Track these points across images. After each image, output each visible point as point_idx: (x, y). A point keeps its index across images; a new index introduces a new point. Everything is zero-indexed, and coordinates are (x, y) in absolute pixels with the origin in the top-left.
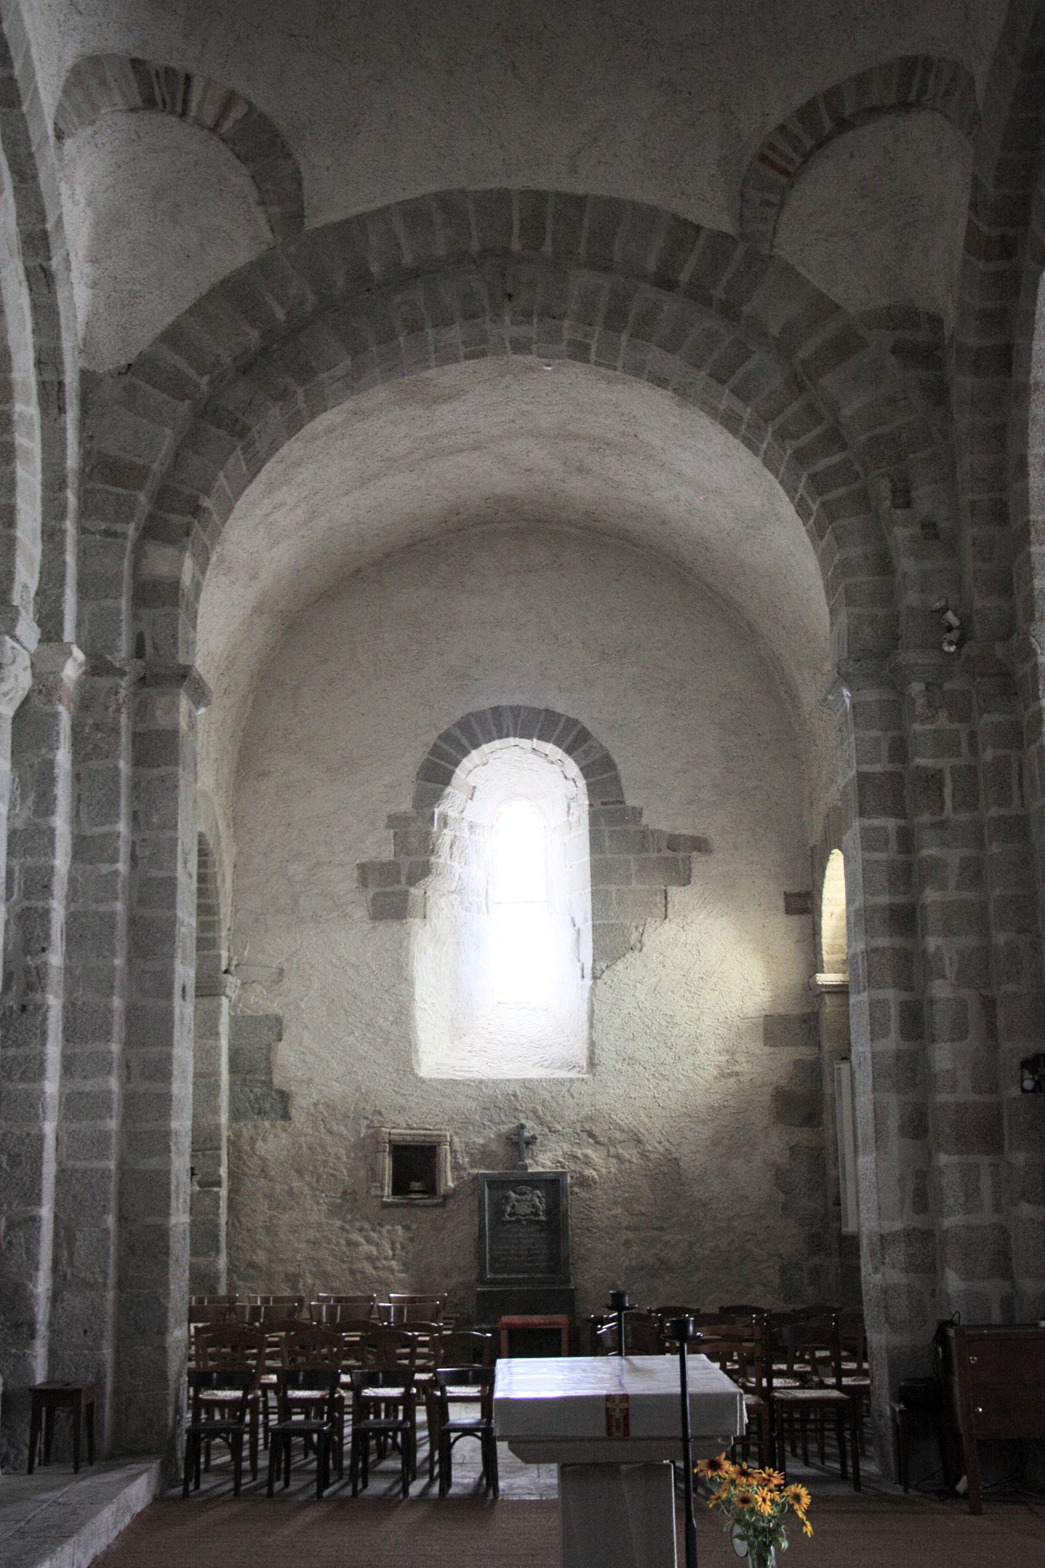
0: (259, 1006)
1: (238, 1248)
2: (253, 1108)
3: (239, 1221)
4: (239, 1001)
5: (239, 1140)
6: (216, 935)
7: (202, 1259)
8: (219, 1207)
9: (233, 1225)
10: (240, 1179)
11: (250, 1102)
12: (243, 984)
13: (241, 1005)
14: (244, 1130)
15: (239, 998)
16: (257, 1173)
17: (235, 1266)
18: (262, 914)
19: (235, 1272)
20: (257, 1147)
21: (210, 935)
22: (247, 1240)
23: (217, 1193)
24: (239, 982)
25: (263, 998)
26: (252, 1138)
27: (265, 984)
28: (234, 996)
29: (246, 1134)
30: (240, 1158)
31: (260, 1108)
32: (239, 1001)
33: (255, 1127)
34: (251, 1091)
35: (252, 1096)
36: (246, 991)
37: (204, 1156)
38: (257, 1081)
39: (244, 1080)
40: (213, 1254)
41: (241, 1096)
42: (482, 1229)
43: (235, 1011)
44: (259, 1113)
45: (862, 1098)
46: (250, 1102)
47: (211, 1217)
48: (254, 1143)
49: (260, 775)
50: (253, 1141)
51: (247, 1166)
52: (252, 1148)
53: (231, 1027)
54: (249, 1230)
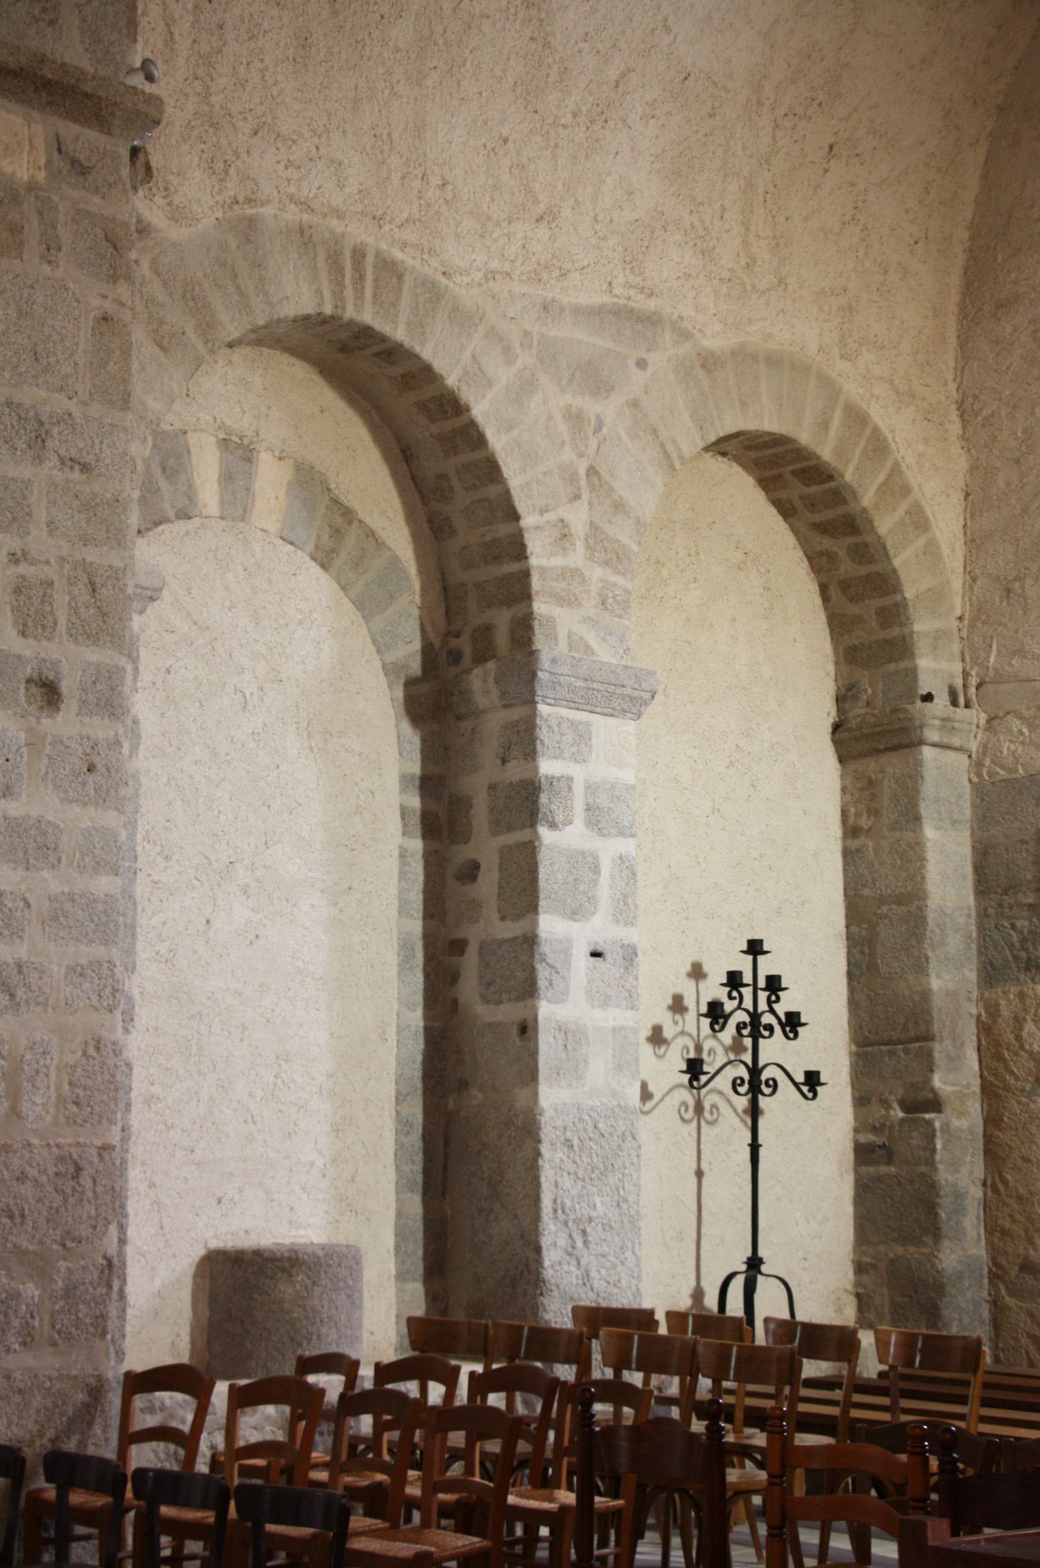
0: (1017, 759)
1: (1005, 1233)
2: (1016, 958)
3: (1005, 1182)
4: (985, 754)
5: (995, 1022)
6: (906, 631)
7: (912, 1249)
8: (934, 1150)
9: (995, 1189)
10: (998, 1096)
11: (1011, 947)
12: (989, 721)
13: (987, 762)
14: (1002, 1002)
15: (984, 748)
16: (1028, 1088)
17: (999, 1266)
18: (1017, 578)
19: (1001, 1279)
20: (1024, 1035)
21: (895, 632)
22: (1018, 1217)
23: (929, 1123)
24: (983, 717)
25: (1023, 743)
26: (1016, 1018)
27: (1026, 714)
28: (974, 746)
29: (1005, 1011)
30: (999, 1057)
31: (1029, 959)
32: (985, 754)
33: (1021, 995)
34: (1013, 927)
35: (1015, 937)
36: (996, 733)
37: (906, 1051)
38: (1021, 905)
39: (1000, 906)
40: (929, 1240)
41: (997, 937)
42: (979, 1234)
43: (979, 775)
44: (1027, 969)
45: (429, 629)
46: (1011, 947)
47: (923, 1169)
48: (1021, 1029)
49: (1000, 306)
50: (1018, 1022)
51: (1012, 1073)
52: (1018, 1038)
53: (974, 806)
54: (1020, 1198)
